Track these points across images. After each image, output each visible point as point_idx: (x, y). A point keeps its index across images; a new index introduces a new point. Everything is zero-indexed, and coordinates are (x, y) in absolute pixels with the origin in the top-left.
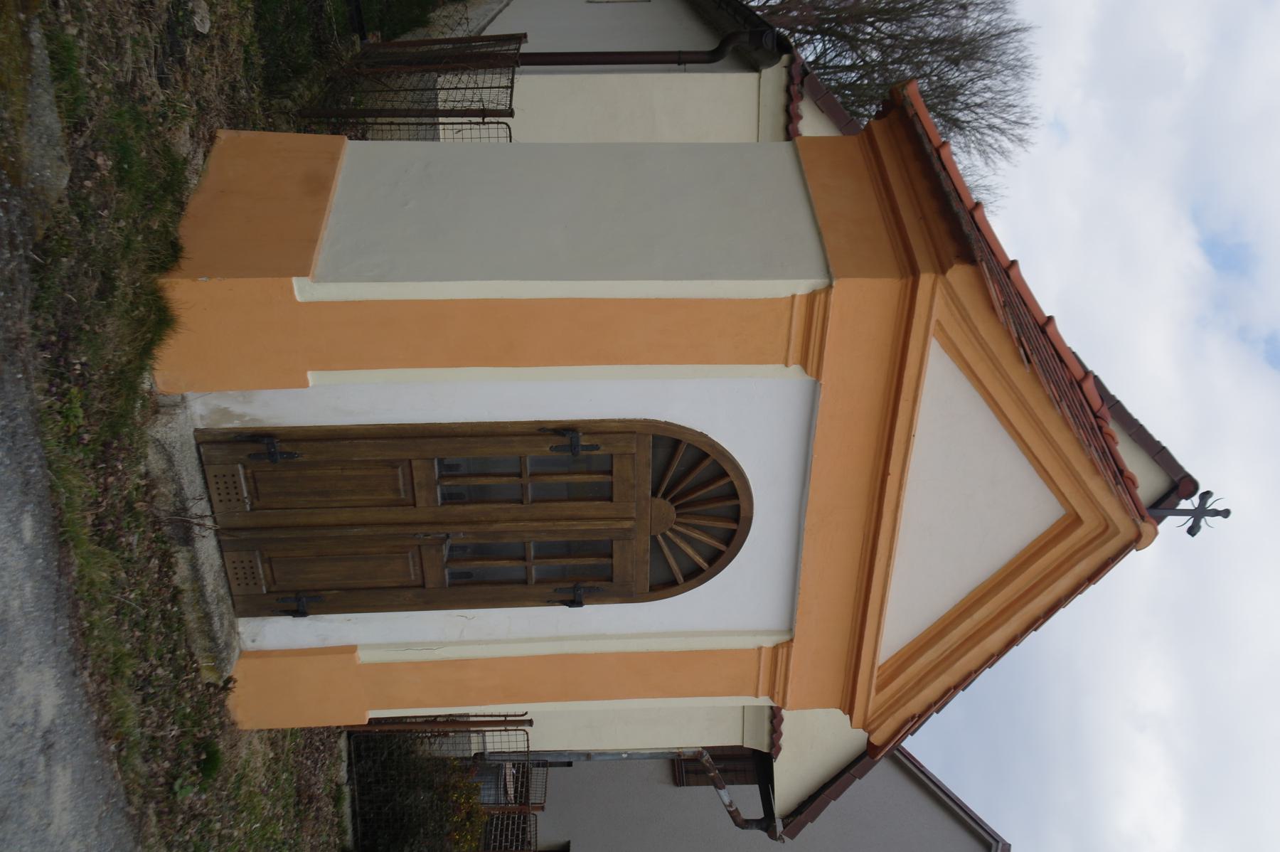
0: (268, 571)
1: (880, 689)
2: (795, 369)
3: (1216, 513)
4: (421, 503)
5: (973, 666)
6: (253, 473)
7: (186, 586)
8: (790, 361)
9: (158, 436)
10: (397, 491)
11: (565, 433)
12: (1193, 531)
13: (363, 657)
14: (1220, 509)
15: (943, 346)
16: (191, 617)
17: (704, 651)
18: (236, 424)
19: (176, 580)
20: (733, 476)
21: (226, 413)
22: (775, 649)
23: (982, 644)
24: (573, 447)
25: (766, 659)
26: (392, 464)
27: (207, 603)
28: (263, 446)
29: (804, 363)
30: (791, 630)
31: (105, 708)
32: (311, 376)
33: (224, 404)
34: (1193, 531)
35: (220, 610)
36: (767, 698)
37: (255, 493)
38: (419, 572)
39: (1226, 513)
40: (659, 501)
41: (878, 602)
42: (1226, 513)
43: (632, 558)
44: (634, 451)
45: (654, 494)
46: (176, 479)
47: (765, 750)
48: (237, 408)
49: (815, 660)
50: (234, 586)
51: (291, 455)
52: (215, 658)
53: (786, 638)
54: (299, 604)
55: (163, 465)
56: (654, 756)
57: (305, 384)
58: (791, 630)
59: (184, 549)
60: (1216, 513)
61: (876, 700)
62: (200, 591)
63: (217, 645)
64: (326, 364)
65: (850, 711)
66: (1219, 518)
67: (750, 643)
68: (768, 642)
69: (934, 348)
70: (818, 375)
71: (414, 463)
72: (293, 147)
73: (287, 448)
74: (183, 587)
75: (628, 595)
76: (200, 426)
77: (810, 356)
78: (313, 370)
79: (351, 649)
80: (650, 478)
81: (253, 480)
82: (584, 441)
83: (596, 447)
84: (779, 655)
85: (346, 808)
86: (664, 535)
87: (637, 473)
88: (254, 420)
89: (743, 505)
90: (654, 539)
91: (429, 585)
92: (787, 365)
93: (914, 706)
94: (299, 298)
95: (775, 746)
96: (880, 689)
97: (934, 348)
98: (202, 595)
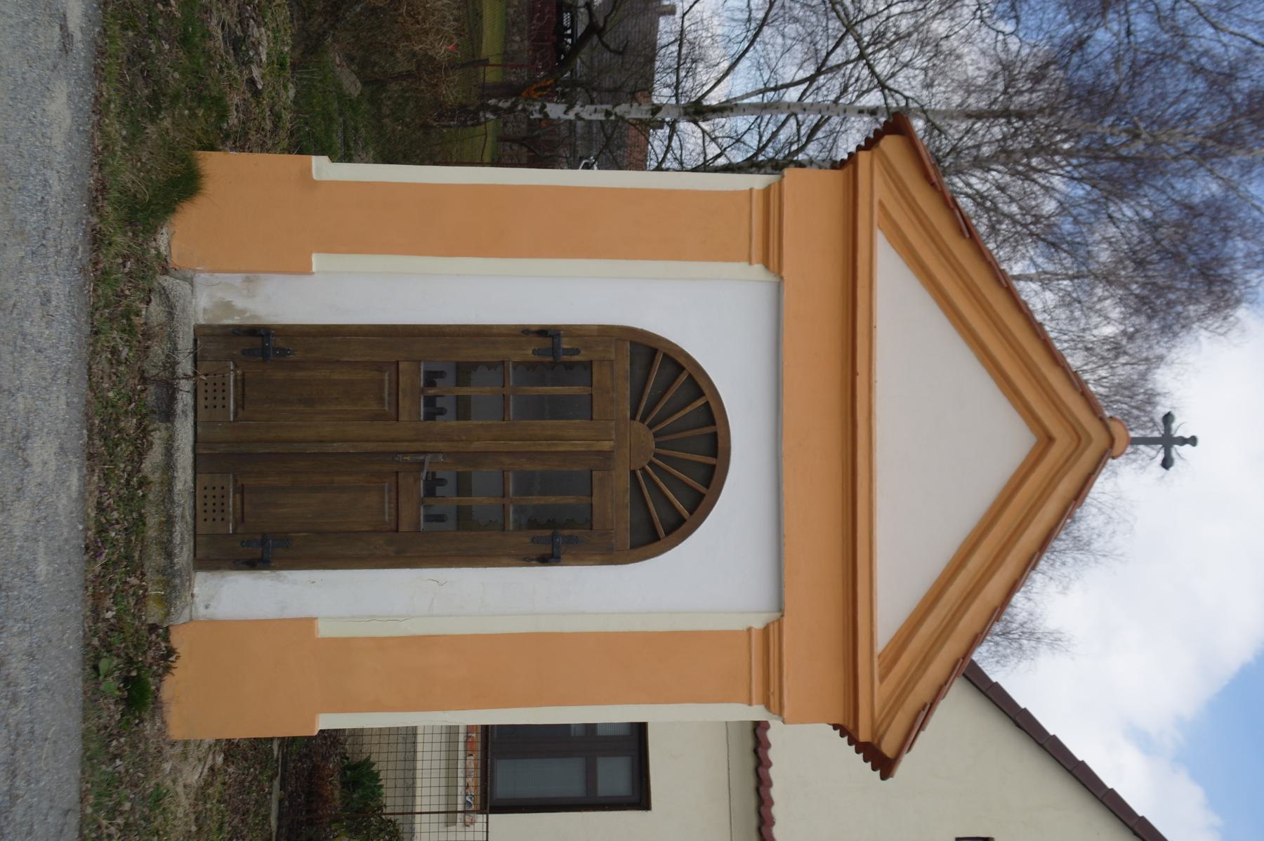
0: (238, 502)
1: (882, 679)
2: (758, 268)
3: (1183, 441)
4: (404, 417)
5: (976, 628)
6: (243, 374)
7: (155, 477)
8: (754, 701)
9: (165, 284)
10: (381, 400)
12: (1167, 463)
13: (324, 630)
14: (1187, 436)
15: (889, 239)
16: (153, 520)
17: (691, 632)
18: (236, 320)
19: (147, 466)
20: (708, 396)
21: (228, 307)
22: (766, 630)
23: (981, 596)
24: (554, 350)
26: (379, 367)
27: (172, 502)
28: (259, 344)
29: (766, 263)
30: (781, 610)
31: (101, 166)
32: (317, 260)
33: (228, 297)
34: (1167, 463)
35: (183, 557)
36: (762, 707)
37: (240, 404)
38: (394, 513)
39: (1193, 441)
40: (637, 424)
41: (866, 549)
42: (1193, 441)
43: (614, 502)
44: (613, 357)
45: (633, 417)
46: (172, 339)
48: (239, 303)
49: (809, 662)
50: (200, 520)
51: (284, 352)
52: (167, 584)
53: (778, 615)
54: (260, 551)
55: (162, 318)
56: (647, 347)
57: (306, 270)
58: (781, 610)
59: (164, 425)
60: (1183, 441)
61: (883, 691)
62: (169, 483)
63: (172, 565)
64: (330, 247)
66: (1188, 446)
67: (737, 624)
68: (758, 625)
70: (779, 272)
71: (402, 366)
73: (281, 343)
74: (151, 478)
75: (610, 554)
76: (202, 322)
77: (770, 254)
78: (318, 251)
79: (310, 621)
80: (628, 393)
81: (242, 383)
82: (565, 344)
83: (577, 352)
84: (770, 637)
86: (643, 469)
87: (616, 383)
88: (255, 317)
89: (720, 434)
90: (633, 473)
91: (403, 528)
92: (750, 263)
93: (922, 691)
94: (315, 177)
96: (882, 679)
98: (170, 491)
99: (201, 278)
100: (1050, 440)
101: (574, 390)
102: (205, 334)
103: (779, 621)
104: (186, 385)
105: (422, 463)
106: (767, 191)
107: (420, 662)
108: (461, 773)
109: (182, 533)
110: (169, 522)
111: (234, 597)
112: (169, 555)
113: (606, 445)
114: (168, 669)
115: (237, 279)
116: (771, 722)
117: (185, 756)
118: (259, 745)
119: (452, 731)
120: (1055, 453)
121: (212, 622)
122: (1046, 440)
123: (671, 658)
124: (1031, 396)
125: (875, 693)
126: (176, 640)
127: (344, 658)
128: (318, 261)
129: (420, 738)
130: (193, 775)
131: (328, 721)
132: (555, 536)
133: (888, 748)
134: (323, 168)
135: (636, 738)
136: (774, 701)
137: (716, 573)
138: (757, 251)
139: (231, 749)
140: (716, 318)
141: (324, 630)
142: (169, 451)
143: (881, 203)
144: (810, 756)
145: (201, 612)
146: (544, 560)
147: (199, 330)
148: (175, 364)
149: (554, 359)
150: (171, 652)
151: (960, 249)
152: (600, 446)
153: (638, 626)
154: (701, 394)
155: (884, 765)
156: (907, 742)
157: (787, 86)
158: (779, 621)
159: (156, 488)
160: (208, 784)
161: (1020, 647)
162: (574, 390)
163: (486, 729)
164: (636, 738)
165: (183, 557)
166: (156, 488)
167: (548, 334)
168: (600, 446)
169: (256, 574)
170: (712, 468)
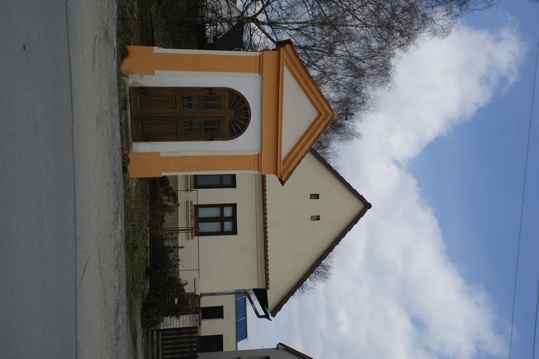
2: (257, 74)
7: (124, 123)
11: (210, 90)
13: (162, 155)
18: (138, 86)
21: (136, 82)
22: (258, 155)
25: (256, 157)
28: (144, 91)
29: (259, 73)
33: (136, 80)
35: (131, 140)
37: (141, 105)
47: (265, 288)
48: (139, 81)
49: (267, 163)
54: (147, 138)
57: (154, 74)
62: (127, 124)
64: (159, 69)
65: (276, 174)
67: (252, 154)
68: (257, 153)
69: (285, 68)
70: (262, 75)
72: (152, 47)
77: (260, 71)
79: (159, 153)
82: (214, 92)
83: (216, 93)
84: (259, 156)
85: (148, 254)
93: (291, 168)
95: (267, 288)
97: (285, 68)
99: (129, 75)
100: (321, 114)
101: (216, 102)
102: (131, 89)
103: (261, 153)
104: (128, 103)
105: (182, 119)
106: (260, 56)
107: (182, 161)
108: (189, 184)
109: (130, 135)
110: (127, 132)
111: (141, 148)
112: (128, 139)
113: (223, 115)
114: (129, 163)
115: (138, 76)
116: (266, 175)
117: (133, 181)
118: (145, 179)
119: (186, 176)
120: (322, 117)
121: (137, 153)
122: (320, 114)
123: (239, 160)
124: (317, 105)
125: (281, 168)
126: (130, 157)
127: (167, 161)
128: (156, 72)
129: (179, 178)
130: (134, 185)
131: (164, 174)
132: (212, 133)
133: (283, 179)
134: (157, 50)
135: (234, 177)
136: (260, 170)
137: (247, 143)
138: (257, 70)
139: (140, 179)
140: (248, 85)
141: (162, 155)
142: (126, 117)
143: (286, 61)
144: (272, 180)
145: (135, 151)
146: (210, 140)
147: (130, 87)
148: (126, 98)
149: (211, 94)
150: (129, 159)
151: (303, 71)
152: (222, 114)
153: (230, 154)
154: (244, 103)
155: (283, 183)
156: (287, 178)
157: (265, 33)
158: (261, 153)
159: (124, 125)
160: (137, 186)
161: (348, 137)
162: (216, 102)
163: (195, 177)
164: (234, 177)
165: (131, 140)
166: (124, 125)
167: (210, 89)
168: (222, 114)
169: (146, 143)
170: (247, 120)
